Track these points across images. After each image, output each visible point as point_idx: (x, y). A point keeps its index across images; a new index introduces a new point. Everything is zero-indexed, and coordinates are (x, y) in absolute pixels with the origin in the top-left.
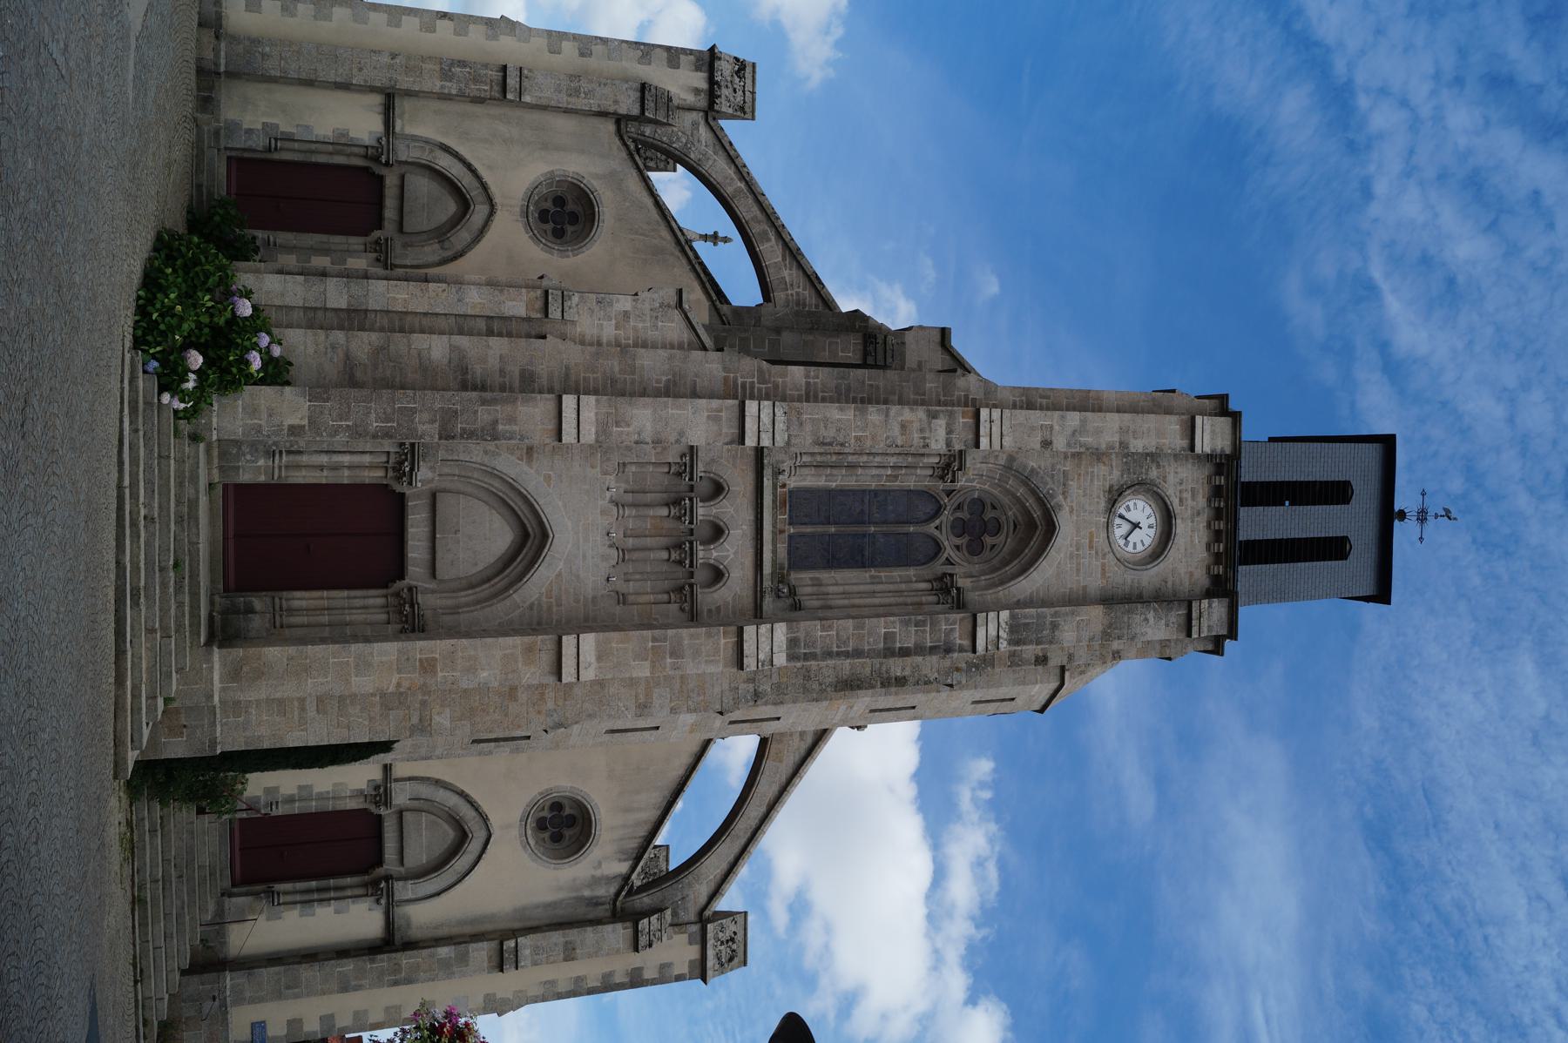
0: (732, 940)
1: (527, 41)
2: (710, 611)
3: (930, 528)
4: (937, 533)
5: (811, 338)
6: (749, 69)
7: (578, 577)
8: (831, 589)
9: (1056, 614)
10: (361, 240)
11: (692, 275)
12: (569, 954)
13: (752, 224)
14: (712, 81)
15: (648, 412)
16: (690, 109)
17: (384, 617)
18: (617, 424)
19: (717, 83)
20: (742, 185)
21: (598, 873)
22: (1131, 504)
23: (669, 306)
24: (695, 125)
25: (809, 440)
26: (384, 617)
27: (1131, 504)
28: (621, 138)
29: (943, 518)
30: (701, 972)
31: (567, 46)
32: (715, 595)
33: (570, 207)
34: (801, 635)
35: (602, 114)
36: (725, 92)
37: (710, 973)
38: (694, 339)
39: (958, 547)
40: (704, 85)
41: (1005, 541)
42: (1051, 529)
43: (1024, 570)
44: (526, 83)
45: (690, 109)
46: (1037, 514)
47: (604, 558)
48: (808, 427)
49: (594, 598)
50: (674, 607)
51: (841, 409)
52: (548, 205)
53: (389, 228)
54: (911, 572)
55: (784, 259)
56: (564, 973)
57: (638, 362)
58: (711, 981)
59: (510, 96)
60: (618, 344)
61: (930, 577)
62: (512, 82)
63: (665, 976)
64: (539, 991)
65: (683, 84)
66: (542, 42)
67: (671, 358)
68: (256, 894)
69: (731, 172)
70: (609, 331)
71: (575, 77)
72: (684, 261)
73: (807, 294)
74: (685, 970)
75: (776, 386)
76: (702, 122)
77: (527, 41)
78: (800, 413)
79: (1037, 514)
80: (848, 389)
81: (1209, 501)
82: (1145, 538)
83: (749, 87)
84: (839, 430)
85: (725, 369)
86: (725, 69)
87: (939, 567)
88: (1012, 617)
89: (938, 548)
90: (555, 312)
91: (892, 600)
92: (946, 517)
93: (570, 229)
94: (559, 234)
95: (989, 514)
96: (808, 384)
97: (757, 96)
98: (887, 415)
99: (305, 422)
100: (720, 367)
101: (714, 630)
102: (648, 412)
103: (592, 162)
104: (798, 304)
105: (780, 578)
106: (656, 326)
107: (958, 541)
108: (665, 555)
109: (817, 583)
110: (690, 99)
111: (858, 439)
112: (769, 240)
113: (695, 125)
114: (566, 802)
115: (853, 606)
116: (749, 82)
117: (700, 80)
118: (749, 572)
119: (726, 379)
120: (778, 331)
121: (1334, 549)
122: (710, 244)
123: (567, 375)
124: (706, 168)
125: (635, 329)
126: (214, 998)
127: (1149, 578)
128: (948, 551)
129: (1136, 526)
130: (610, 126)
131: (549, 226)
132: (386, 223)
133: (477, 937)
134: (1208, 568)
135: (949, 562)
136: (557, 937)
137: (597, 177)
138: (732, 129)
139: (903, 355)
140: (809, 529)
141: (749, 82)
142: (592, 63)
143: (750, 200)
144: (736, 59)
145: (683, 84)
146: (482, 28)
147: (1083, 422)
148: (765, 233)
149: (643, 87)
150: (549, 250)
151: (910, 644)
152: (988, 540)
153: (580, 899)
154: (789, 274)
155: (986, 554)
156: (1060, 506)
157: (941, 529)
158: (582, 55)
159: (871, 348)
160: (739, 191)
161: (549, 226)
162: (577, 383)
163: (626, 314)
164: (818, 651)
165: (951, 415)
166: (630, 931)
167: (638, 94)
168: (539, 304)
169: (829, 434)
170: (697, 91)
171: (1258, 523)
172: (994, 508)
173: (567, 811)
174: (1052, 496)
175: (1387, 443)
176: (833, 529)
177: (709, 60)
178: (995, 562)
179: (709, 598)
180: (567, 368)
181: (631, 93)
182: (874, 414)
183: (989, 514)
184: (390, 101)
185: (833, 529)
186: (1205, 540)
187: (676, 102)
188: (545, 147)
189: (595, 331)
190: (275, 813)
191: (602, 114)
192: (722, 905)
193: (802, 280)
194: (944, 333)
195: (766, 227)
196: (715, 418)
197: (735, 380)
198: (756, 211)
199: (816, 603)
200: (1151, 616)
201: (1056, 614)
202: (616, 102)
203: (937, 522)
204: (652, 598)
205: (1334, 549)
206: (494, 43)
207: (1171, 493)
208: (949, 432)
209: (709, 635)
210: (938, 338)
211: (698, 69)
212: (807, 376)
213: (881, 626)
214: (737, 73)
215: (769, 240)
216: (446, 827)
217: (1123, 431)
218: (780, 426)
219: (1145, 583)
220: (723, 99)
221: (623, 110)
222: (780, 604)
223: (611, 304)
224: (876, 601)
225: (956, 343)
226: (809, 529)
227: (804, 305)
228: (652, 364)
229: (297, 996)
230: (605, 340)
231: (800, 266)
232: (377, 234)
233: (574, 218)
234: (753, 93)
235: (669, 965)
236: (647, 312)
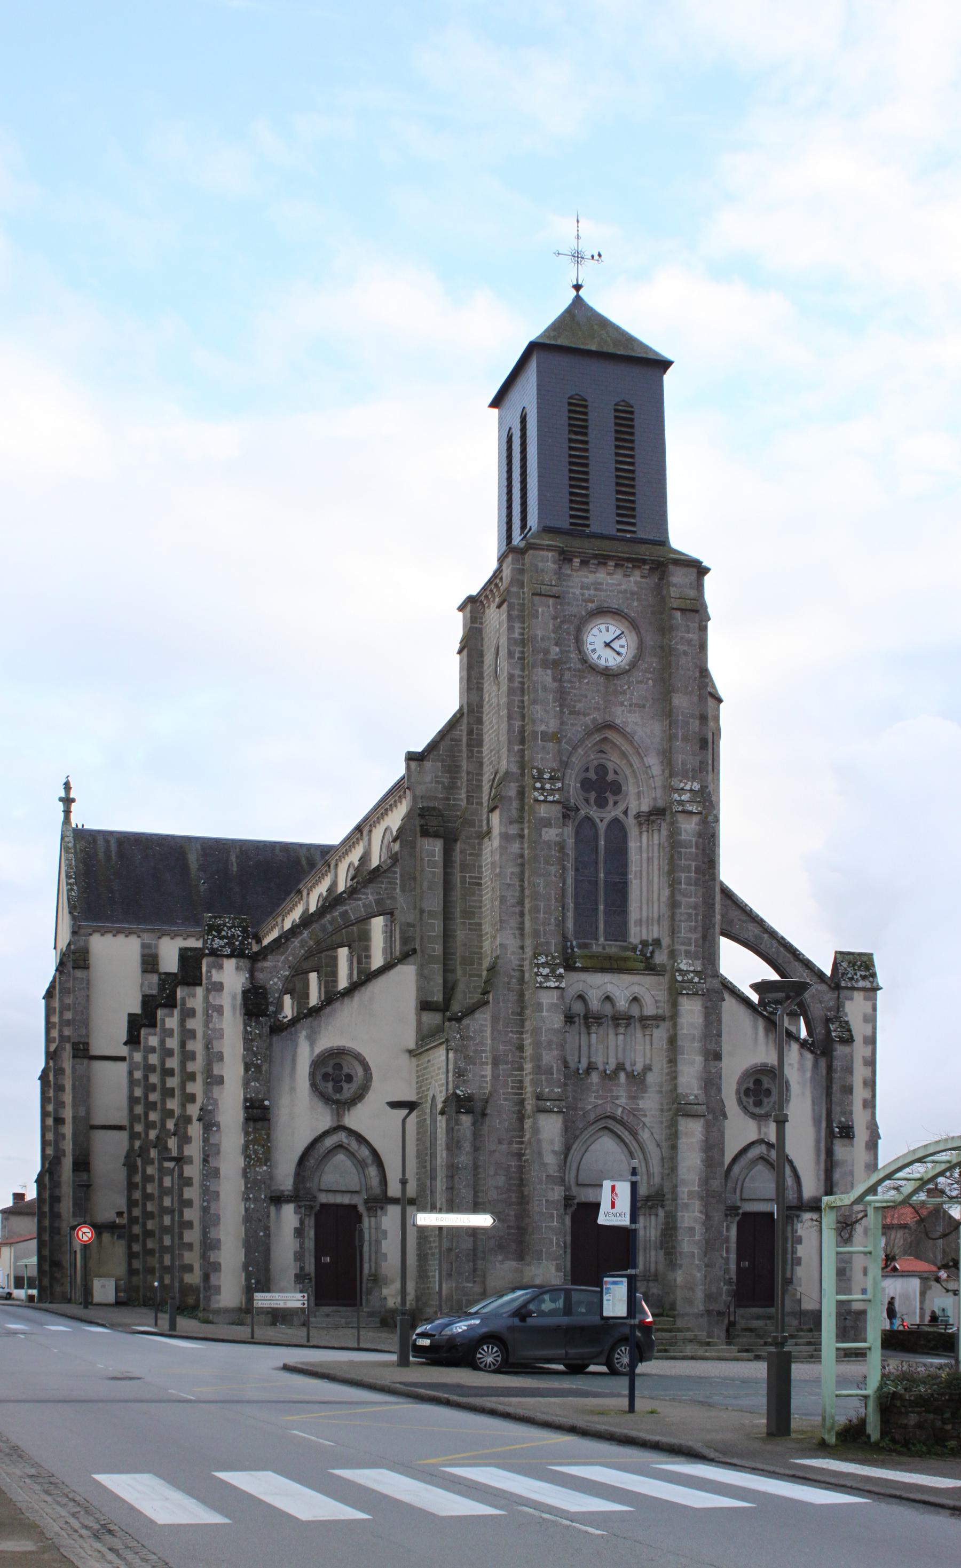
3: (602, 827)
4: (603, 815)
8: (644, 914)
10: (366, 1220)
12: (849, 1090)
17: (653, 1217)
21: (796, 1066)
22: (591, 647)
26: (653, 1217)
27: (591, 647)
33: (330, 1070)
50: (655, 1031)
53: (358, 1200)
54: (633, 845)
56: (860, 1093)
63: (871, 1019)
64: (869, 1111)
68: (784, 1292)
74: (869, 1004)
92: (594, 813)
95: (592, 775)
99: (554, 1263)
107: (611, 803)
108: (621, 1037)
109: (639, 922)
112: (346, 911)
114: (745, 1086)
120: (422, 911)
122: (74, 806)
126: (846, 1319)
128: (617, 812)
129: (607, 645)
132: (353, 1202)
133: (830, 1153)
136: (837, 1096)
137: (312, 1050)
140: (601, 926)
153: (813, 1079)
171: (603, 517)
172: (587, 770)
173: (751, 1085)
176: (602, 907)
183: (592, 775)
184: (278, 1200)
185: (602, 907)
190: (735, 1280)
192: (828, 972)
203: (598, 821)
204: (648, 1047)
210: (413, 764)
215: (346, 911)
216: (754, 1171)
225: (419, 748)
226: (601, 926)
229: (851, 1270)
232: (361, 1209)
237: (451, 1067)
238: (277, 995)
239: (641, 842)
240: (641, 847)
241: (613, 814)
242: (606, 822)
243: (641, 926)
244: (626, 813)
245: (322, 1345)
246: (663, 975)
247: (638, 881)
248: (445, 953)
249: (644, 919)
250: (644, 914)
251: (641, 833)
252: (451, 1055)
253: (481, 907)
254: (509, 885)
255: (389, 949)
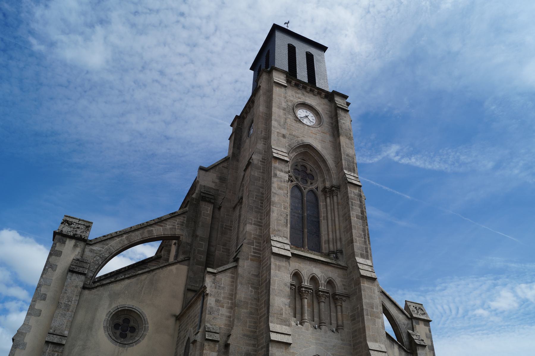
0: (416, 308)
1: (30, 327)
2: (345, 289)
5: (200, 223)
6: (68, 219)
7: (334, 346)
9: (344, 153)
11: (165, 269)
13: (144, 236)
14: (73, 237)
15: (277, 298)
16: (83, 251)
18: (282, 314)
19: (74, 235)
20: (125, 236)
23: (214, 279)
24: (91, 251)
25: (285, 229)
28: (93, 288)
29: (301, 186)
30: (427, 322)
31: (38, 306)
32: (339, 285)
33: (121, 321)
34: (359, 252)
35: (81, 294)
36: (79, 232)
37: (428, 319)
38: (230, 271)
39: (311, 184)
40: (73, 242)
41: (310, 165)
42: (309, 146)
43: (324, 161)
44: (58, 332)
45: (83, 251)
46: (302, 150)
47: (326, 332)
48: (280, 228)
49: (342, 340)
50: (344, 304)
51: (273, 212)
52: (118, 332)
55: (162, 226)
57: (243, 299)
58: (430, 319)
59: (64, 342)
60: (231, 308)
61: (323, 196)
62: (56, 340)
65: (70, 252)
66: (33, 320)
67: (241, 284)
69: (118, 239)
70: (224, 311)
71: (58, 305)
72: (158, 271)
73: (178, 220)
74: (427, 328)
75: (255, 238)
76: (91, 247)
77: (30, 327)
78: (274, 230)
79: (302, 150)
80: (257, 208)
81: (299, 89)
82: (312, 117)
83: (77, 221)
84: (281, 215)
85: (247, 259)
86: (66, 229)
87: (319, 193)
88: (346, 169)
89: (312, 191)
90: (216, 337)
91: (336, 213)
93: (132, 324)
94: (133, 330)
96: (254, 224)
97: (82, 218)
98: (275, 194)
100: (246, 261)
101: (362, 287)
102: (277, 298)
103: (104, 305)
104: (182, 225)
105: (327, 255)
106: (223, 288)
107: (309, 183)
110: (78, 250)
111: (285, 208)
112: (152, 230)
113: (91, 251)
115: (339, 229)
116: (74, 220)
117: (70, 243)
118: (329, 269)
119: (251, 260)
121: (310, 58)
123: (247, 336)
124: (113, 250)
125: (224, 298)
127: (326, 119)
130: (86, 292)
131: (129, 334)
134: (322, 98)
135: (317, 188)
137: (110, 305)
138: (92, 235)
139: (209, 188)
141: (74, 220)
142: (50, 294)
143: (133, 234)
144: (62, 223)
145: (70, 252)
146: (18, 351)
147: (276, 120)
148: (149, 231)
149: (71, 271)
150: (143, 336)
151: (359, 210)
152: (308, 172)
154: (168, 226)
155: (314, 174)
156: (302, 140)
157: (307, 188)
158: (44, 299)
159: (208, 199)
160: (127, 238)
161: (129, 334)
162: (252, 331)
163: (217, 301)
164: (365, 246)
165: (275, 168)
166: (420, 348)
167: (74, 274)
168: (212, 344)
169: (283, 221)
170: (75, 246)
174: (298, 142)
175: (275, 28)
177: (59, 236)
178: (317, 171)
179: (340, 288)
180: (244, 335)
181: (73, 278)
182: (275, 199)
186: (312, 95)
187: (79, 257)
188: (90, 328)
189: (224, 318)
191: (81, 294)
193: (172, 220)
194: (201, 168)
195: (146, 230)
196: (279, 268)
197: (253, 256)
198: (137, 233)
199: (339, 244)
200: (343, 121)
201: (344, 153)
202: (76, 287)
204: (339, 314)
205: (310, 58)
206: (27, 346)
207: (297, 101)
208: (282, 171)
209: (364, 290)
210: (202, 172)
211: (64, 243)
212: (251, 224)
213: (354, 219)
214: (69, 224)
215: (152, 230)
217: (279, 108)
218: (280, 239)
219: (327, 120)
220: (83, 234)
221: (81, 284)
222: (340, 258)
223: (212, 308)
224: (337, 219)
225: (206, 165)
227: (183, 222)
228: (244, 293)
230: (228, 314)
231: (166, 220)
233: (127, 321)
234: (80, 220)
235: (426, 334)
236: (216, 290)
237: (207, 196)
238: (96, 267)
239: (326, 202)
240: (326, 205)
241: (311, 187)
242: (307, 190)
243: (329, 243)
244: (317, 188)
245: (376, 352)
246: (346, 270)
247: (326, 221)
248: (207, 260)
249: (331, 239)
250: (331, 236)
251: (326, 198)
252: (209, 270)
253: (230, 241)
254: (254, 201)
255: (176, 256)
